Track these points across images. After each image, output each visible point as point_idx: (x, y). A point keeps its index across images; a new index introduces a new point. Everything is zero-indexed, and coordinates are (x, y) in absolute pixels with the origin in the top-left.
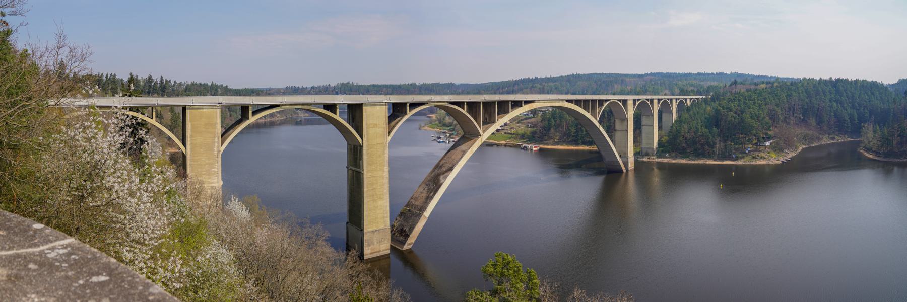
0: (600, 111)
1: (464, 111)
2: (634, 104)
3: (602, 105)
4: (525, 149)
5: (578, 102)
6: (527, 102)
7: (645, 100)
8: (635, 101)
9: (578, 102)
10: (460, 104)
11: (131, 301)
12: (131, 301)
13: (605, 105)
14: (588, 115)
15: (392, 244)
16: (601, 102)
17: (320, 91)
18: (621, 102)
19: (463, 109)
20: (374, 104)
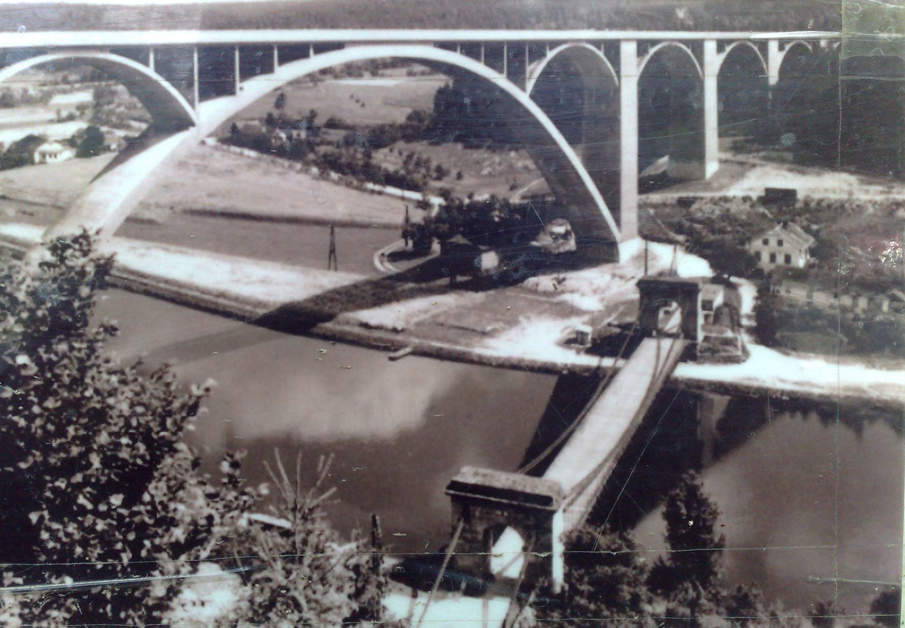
0: (536, 69)
1: (149, 71)
2: (781, 48)
3: (543, 55)
4: (380, 193)
5: (470, 49)
6: (322, 48)
7: (802, 42)
8: (782, 43)
9: (470, 49)
10: (137, 52)
11: (903, 79)
12: (903, 79)
13: (550, 54)
14: (501, 80)
15: (621, 353)
16: (537, 49)
17: (230, 23)
18: (599, 48)
19: (146, 63)
20: (628, 40)
